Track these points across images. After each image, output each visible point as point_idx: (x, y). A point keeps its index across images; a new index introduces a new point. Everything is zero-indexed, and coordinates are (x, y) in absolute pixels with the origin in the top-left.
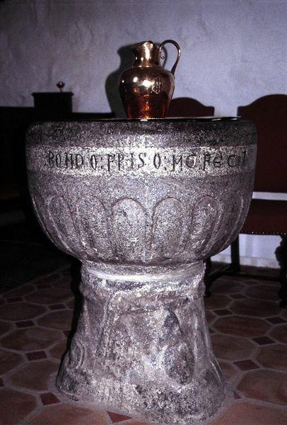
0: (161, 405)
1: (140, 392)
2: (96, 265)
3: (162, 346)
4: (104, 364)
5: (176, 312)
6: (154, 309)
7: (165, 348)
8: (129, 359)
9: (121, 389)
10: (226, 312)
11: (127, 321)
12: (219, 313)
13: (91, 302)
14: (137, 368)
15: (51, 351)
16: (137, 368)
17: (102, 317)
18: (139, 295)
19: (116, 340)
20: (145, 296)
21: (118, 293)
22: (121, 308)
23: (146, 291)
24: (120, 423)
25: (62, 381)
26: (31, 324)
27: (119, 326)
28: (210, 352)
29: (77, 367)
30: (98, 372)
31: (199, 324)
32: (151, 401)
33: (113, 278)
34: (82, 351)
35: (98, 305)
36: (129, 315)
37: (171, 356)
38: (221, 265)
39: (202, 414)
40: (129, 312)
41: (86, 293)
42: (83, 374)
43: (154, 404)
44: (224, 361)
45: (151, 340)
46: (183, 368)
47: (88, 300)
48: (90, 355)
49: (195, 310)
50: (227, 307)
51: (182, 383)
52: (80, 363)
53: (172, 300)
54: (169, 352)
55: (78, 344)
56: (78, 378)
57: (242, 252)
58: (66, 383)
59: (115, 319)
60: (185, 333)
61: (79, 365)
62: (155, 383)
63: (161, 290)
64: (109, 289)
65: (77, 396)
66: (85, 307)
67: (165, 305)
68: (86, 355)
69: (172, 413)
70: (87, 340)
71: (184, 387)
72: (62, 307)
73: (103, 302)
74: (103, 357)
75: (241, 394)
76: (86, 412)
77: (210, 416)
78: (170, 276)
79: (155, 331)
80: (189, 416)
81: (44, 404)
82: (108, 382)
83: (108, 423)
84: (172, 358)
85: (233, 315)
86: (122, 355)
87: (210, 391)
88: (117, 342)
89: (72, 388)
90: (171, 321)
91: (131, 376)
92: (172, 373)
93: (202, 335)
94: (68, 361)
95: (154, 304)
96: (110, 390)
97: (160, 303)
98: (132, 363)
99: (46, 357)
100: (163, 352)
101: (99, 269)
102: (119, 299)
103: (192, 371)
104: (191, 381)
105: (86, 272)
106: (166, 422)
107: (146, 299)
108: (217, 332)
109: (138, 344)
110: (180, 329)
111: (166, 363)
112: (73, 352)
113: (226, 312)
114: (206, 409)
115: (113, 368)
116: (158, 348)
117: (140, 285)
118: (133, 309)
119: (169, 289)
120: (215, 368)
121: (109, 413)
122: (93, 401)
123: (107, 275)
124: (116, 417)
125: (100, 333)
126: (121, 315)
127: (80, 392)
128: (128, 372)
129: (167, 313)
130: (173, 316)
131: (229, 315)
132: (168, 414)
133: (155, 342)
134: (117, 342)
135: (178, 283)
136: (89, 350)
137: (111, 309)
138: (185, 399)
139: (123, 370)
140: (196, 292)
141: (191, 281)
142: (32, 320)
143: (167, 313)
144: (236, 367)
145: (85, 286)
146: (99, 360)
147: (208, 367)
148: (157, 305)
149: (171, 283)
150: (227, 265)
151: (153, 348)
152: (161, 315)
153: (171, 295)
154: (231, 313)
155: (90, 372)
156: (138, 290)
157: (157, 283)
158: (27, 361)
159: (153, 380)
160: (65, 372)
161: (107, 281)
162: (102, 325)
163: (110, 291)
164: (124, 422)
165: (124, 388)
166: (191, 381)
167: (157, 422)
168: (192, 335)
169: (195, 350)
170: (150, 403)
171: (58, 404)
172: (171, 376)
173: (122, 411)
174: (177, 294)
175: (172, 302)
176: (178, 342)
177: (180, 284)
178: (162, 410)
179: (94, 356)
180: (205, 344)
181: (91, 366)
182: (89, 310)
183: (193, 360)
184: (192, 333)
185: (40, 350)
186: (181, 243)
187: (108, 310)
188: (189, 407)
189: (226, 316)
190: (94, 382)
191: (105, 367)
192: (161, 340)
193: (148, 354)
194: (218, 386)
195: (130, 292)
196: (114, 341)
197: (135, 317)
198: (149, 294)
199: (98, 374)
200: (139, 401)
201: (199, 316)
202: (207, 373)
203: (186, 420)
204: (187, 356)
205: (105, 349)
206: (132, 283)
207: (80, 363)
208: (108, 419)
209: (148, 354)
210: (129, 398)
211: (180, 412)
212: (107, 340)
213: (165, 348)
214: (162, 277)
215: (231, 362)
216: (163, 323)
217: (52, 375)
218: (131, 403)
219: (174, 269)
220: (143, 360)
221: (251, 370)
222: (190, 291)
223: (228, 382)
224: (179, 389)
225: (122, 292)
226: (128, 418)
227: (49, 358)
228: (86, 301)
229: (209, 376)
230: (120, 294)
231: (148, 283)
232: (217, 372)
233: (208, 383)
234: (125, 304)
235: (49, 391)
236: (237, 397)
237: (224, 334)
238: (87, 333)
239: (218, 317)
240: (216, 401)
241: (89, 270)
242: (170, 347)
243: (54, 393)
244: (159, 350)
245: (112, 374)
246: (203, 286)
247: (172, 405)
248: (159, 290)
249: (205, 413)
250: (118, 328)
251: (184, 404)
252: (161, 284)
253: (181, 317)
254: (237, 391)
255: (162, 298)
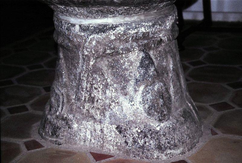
0: (141, 142)
1: (120, 132)
2: (67, 10)
3: (139, 86)
4: (84, 108)
5: (151, 53)
6: (128, 50)
7: (142, 88)
8: (107, 101)
9: (102, 131)
10: (200, 63)
11: (104, 64)
12: (193, 64)
13: (66, 49)
14: (116, 109)
15: (32, 105)
16: (116, 109)
17: (78, 63)
18: (113, 38)
19: (93, 84)
20: (119, 38)
21: (92, 37)
22: (97, 51)
23: (119, 33)
24: (103, 161)
25: (44, 127)
26: (11, 83)
27: (96, 70)
28: (186, 94)
29: (58, 113)
30: (78, 116)
31: (174, 65)
32: (131, 140)
33: (86, 22)
34: (61, 97)
35: (73, 52)
36: (104, 59)
37: (148, 95)
38: (193, 24)
39: (181, 149)
40: (104, 55)
41: (60, 40)
42: (64, 119)
43: (135, 142)
44: (201, 104)
45: (127, 81)
46: (160, 107)
47: (63, 47)
48: (69, 100)
49: (169, 52)
50: (201, 59)
51: (160, 121)
52: (60, 109)
53: (146, 41)
54: (146, 92)
55: (57, 91)
56: (60, 123)
57: (214, 7)
58: (49, 130)
59: (92, 63)
60: (160, 74)
61: (60, 111)
62: (134, 122)
63: (134, 32)
64: (83, 34)
65: (59, 140)
66: (61, 55)
67: (139, 46)
68: (65, 101)
69: (152, 149)
70: (66, 86)
71: (162, 125)
72: (41, 67)
73: (78, 47)
74: (82, 101)
75: (218, 131)
76: (69, 154)
77: (189, 150)
78: (142, 18)
79: (131, 72)
80: (169, 151)
81: (28, 150)
82: (89, 124)
83: (92, 162)
84: (149, 97)
85: (207, 65)
86: (100, 97)
87: (188, 128)
88: (95, 86)
89: (55, 131)
90: (146, 63)
91: (110, 117)
92: (150, 112)
93: (178, 75)
94: (49, 108)
95: (128, 45)
96: (91, 132)
97: (135, 44)
98: (110, 105)
99: (27, 110)
100: (140, 92)
101: (71, 14)
102: (94, 43)
103: (169, 109)
104: (169, 119)
105: (58, 19)
106: (147, 157)
107: (120, 41)
108: (192, 81)
109: (115, 85)
110: (156, 70)
111: (144, 102)
112: (53, 100)
113: (200, 63)
114: (185, 144)
115: (92, 111)
116: (135, 88)
117: (113, 28)
118: (108, 51)
119: (143, 30)
120: (192, 108)
121: (92, 154)
122: (75, 144)
123: (79, 20)
124: (98, 157)
125: (78, 78)
126: (97, 58)
127: (63, 136)
128: (107, 114)
129: (142, 55)
130: (147, 57)
131: (203, 65)
132: (149, 150)
133: (132, 82)
134: (95, 86)
135: (151, 24)
136: (68, 96)
137: (86, 53)
138: (164, 135)
139: (103, 113)
140: (170, 33)
141: (164, 22)
142: (26, 104)
143: (142, 55)
144: (212, 109)
145: (60, 33)
146: (79, 104)
147: (184, 107)
148: (132, 47)
149: (144, 24)
150: (199, 21)
151: (130, 89)
152: (136, 56)
153: (145, 36)
154: (204, 64)
155: (71, 116)
156: (112, 32)
157: (130, 25)
158: (9, 115)
159: (132, 119)
160: (46, 120)
161: (80, 26)
162: (79, 70)
163: (84, 36)
164: (108, 160)
165: (105, 129)
166: (169, 119)
167: (138, 158)
168: (168, 75)
169: (172, 90)
170: (130, 141)
171: (43, 149)
172: (149, 114)
173: (105, 151)
174: (151, 35)
175: (146, 43)
176: (154, 82)
177: (153, 25)
178: (143, 147)
179: (73, 101)
180: (180, 85)
181: (71, 111)
182: (65, 57)
183: (169, 98)
184: (167, 74)
185: (21, 105)
186: (163, 44)
187: (83, 55)
188: (168, 143)
189: (201, 66)
190: (75, 126)
191: (85, 111)
192: (137, 81)
193: (126, 95)
194: (195, 123)
195: (104, 35)
196: (92, 85)
197: (110, 60)
198: (123, 35)
199: (78, 117)
200: (120, 140)
201: (174, 57)
202: (184, 112)
203: (166, 155)
204: (163, 95)
205: (83, 93)
206: (105, 26)
207: (60, 109)
208: (91, 158)
209: (126, 95)
210: (110, 139)
211: (160, 148)
212: (84, 84)
213: (142, 88)
214: (135, 18)
215: (207, 105)
216: (138, 64)
217: (35, 125)
218: (112, 141)
219: (146, 10)
220: (120, 100)
221: (226, 111)
222: (163, 32)
223: (205, 122)
224: (157, 126)
225: (96, 36)
226: (111, 156)
227: (31, 111)
228: (61, 49)
229: (186, 115)
230: (94, 38)
231: (121, 25)
232: (194, 111)
233: (186, 121)
234: (100, 47)
235: (32, 139)
236: (214, 133)
237: (199, 82)
238: (65, 80)
239: (192, 67)
240: (194, 138)
241: (62, 17)
242: (147, 86)
243: (37, 140)
244: (136, 91)
245: (92, 117)
246: (177, 28)
247: (151, 142)
248: (132, 32)
249: (184, 148)
250: (95, 72)
251: (163, 141)
252: (134, 25)
253: (156, 58)
254: (214, 129)
255: (136, 39)
